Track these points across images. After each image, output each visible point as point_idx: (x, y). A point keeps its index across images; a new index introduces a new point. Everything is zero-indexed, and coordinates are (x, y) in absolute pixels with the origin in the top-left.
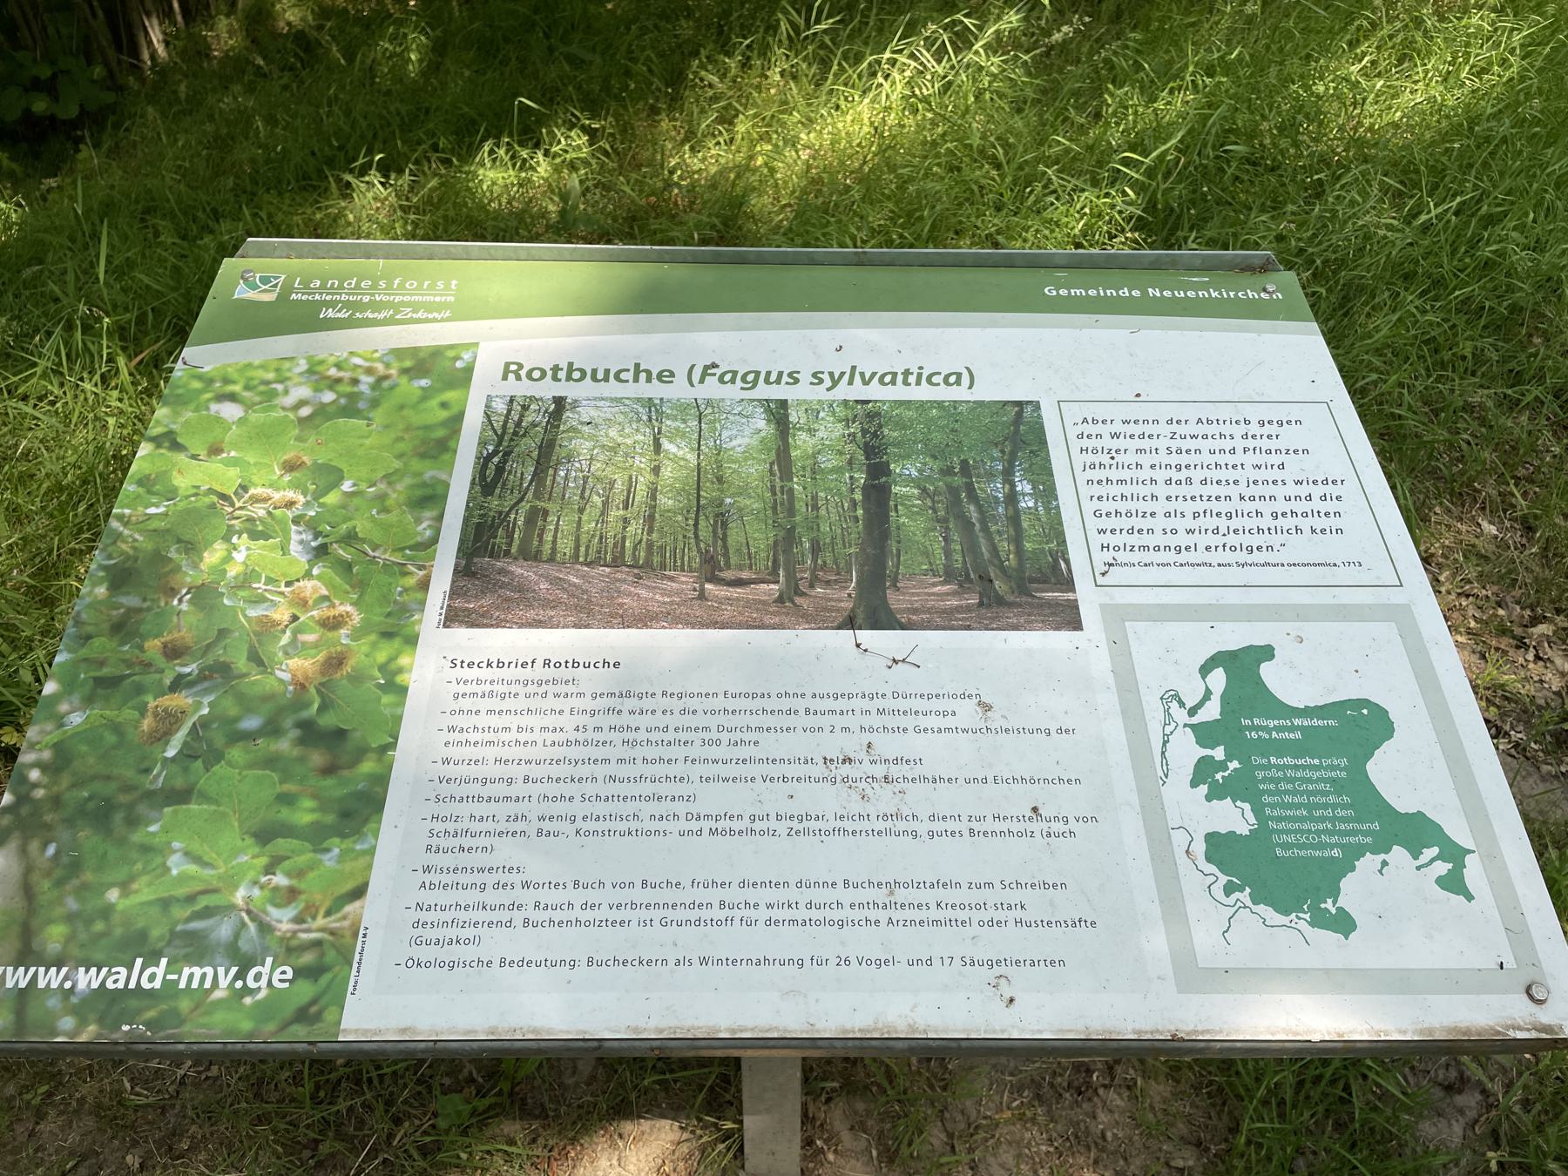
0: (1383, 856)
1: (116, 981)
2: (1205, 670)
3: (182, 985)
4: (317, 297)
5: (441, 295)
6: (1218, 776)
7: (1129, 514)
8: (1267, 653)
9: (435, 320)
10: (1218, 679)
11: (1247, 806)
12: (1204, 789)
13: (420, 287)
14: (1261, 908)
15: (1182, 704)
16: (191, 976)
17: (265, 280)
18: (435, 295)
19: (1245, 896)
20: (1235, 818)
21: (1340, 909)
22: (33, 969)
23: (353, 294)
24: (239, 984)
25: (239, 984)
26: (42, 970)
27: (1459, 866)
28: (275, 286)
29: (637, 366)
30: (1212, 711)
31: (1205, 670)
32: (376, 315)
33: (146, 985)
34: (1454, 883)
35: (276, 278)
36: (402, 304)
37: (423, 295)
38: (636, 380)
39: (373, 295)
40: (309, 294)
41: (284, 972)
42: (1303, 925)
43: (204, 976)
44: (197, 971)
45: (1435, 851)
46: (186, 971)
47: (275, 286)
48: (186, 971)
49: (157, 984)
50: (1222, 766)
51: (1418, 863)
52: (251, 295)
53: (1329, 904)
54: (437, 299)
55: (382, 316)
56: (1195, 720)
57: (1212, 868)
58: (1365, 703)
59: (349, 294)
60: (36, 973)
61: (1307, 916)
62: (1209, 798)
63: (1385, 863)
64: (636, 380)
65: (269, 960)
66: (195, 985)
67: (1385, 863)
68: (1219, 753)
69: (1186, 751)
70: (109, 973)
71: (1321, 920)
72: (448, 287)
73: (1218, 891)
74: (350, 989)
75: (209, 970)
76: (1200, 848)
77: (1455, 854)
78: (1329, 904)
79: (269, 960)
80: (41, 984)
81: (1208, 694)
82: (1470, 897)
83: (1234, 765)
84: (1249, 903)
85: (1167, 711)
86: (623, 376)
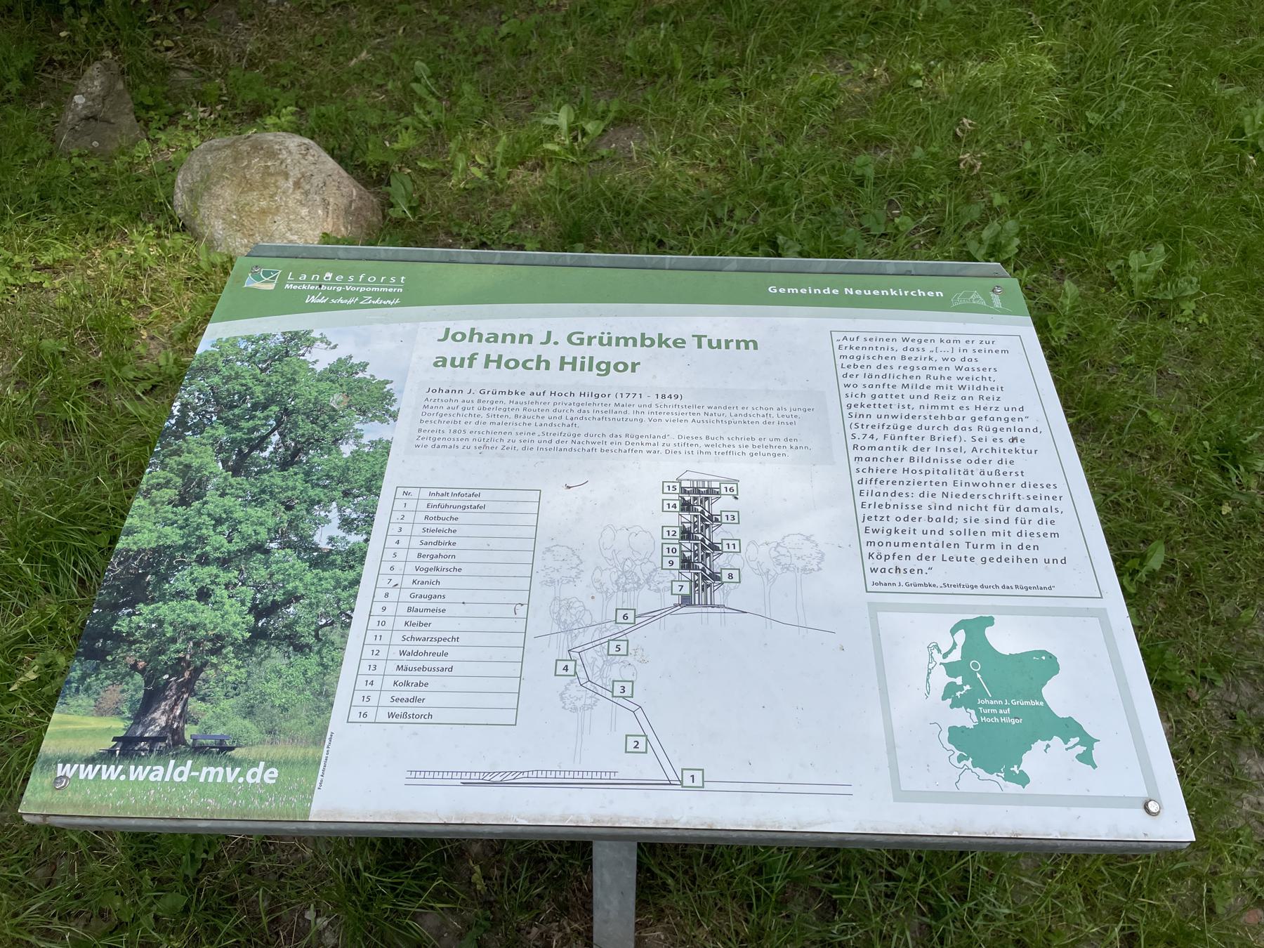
0: (1047, 742)
1: (156, 776)
2: (953, 631)
3: (202, 780)
4: (304, 287)
5: (393, 287)
6: (958, 694)
7: (868, 459)
8: (990, 621)
9: (388, 306)
10: (961, 637)
11: (973, 712)
12: (949, 701)
13: (378, 281)
14: (978, 770)
15: (939, 651)
16: (208, 773)
17: (267, 274)
18: (389, 287)
19: (969, 763)
20: (964, 718)
21: (1021, 772)
22: (98, 767)
23: (330, 285)
24: (241, 780)
25: (241, 780)
26: (82, 766)
27: (1090, 748)
28: (274, 278)
29: (539, 357)
30: (956, 656)
31: (953, 631)
32: (346, 301)
33: (177, 779)
34: (1086, 758)
35: (274, 272)
36: (366, 293)
37: (380, 287)
38: (538, 368)
39: (344, 286)
40: (298, 285)
41: (272, 773)
42: (1000, 780)
43: (217, 773)
44: (212, 770)
45: (1077, 739)
46: (205, 770)
47: (274, 278)
48: (205, 770)
49: (185, 778)
50: (960, 688)
51: (1067, 746)
52: (257, 285)
53: (1015, 768)
54: (390, 290)
55: (350, 302)
56: (947, 661)
57: (952, 747)
58: (1044, 652)
59: (326, 285)
60: (100, 769)
61: (1003, 775)
62: (952, 706)
63: (1048, 746)
64: (538, 368)
65: (262, 764)
66: (211, 780)
67: (1048, 746)
68: (959, 681)
69: (941, 679)
70: (151, 771)
71: (1010, 777)
72: (398, 281)
73: (954, 759)
74: (318, 785)
75: (220, 769)
76: (945, 735)
77: (1088, 741)
78: (1015, 768)
79: (262, 764)
80: (82, 776)
81: (954, 645)
82: (1095, 766)
83: (967, 687)
84: (971, 767)
85: (931, 655)
86: (529, 364)
